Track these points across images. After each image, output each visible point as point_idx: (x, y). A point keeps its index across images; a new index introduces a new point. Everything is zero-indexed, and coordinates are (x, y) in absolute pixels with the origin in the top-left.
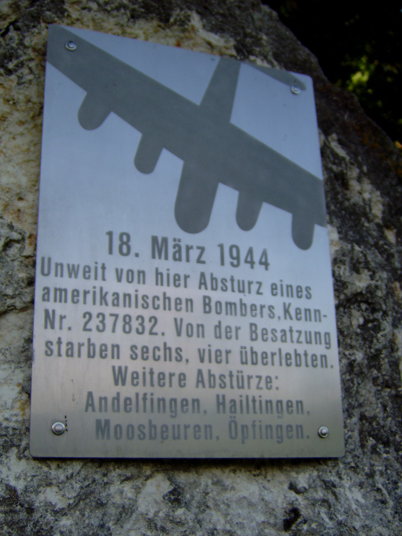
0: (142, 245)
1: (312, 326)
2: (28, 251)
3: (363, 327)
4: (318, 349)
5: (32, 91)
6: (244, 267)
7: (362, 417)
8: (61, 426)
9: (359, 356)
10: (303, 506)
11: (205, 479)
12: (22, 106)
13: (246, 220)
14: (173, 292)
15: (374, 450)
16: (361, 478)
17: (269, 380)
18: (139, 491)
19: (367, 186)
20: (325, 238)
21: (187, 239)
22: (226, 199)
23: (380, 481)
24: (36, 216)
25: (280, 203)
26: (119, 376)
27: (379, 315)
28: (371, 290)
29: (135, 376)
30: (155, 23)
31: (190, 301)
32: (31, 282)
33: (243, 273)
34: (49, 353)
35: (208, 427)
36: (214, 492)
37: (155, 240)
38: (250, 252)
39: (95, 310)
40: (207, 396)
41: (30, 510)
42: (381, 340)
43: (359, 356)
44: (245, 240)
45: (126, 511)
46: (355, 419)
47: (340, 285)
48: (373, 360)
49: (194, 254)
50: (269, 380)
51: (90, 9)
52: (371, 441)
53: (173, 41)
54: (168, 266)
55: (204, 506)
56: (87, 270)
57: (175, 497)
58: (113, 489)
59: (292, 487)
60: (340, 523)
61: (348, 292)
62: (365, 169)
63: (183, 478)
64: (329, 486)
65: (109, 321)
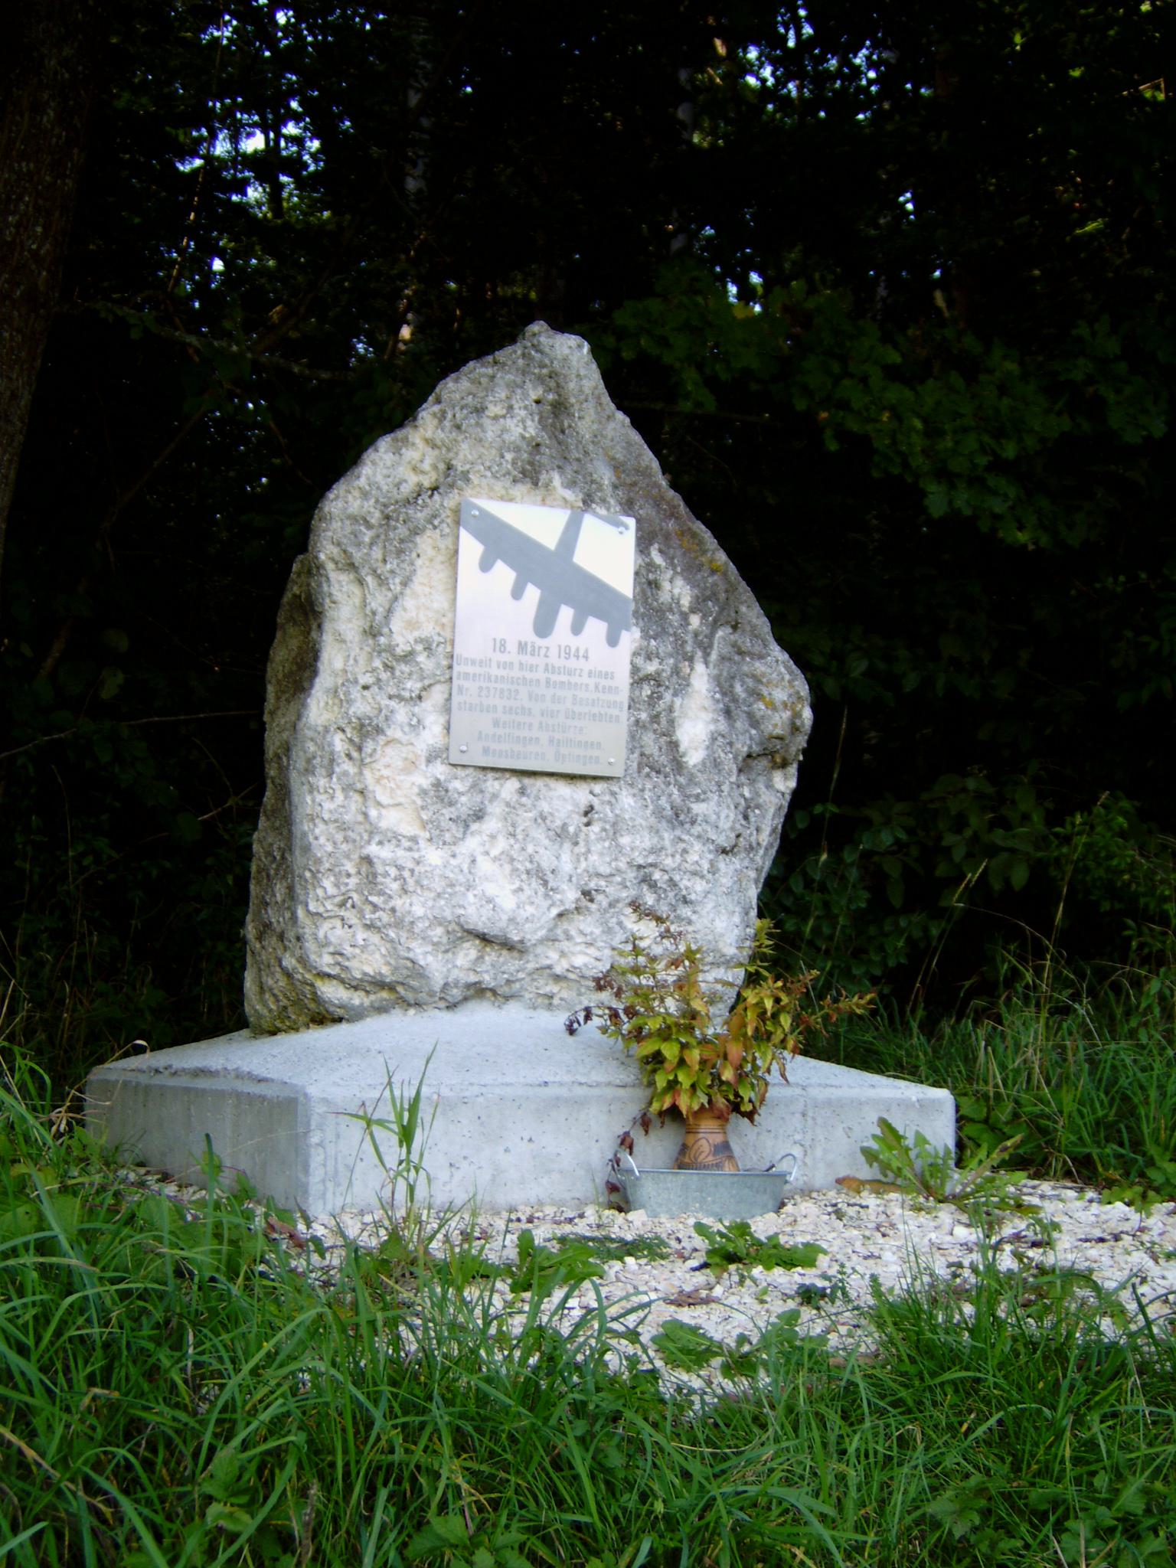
0: (512, 647)
1: (611, 697)
2: (449, 649)
3: (650, 697)
4: (615, 712)
5: (449, 541)
6: (573, 659)
7: (642, 754)
8: (464, 748)
9: (644, 716)
10: (943, 924)
11: (540, 783)
12: (443, 552)
13: (577, 628)
14: (529, 675)
15: (648, 775)
16: (635, 791)
17: (581, 729)
18: (233, 1074)
19: (679, 582)
20: (631, 638)
21: (540, 642)
22: (566, 614)
23: (647, 795)
24: (454, 627)
25: (600, 616)
26: (496, 723)
27: (662, 689)
28: (658, 673)
29: (505, 723)
30: (529, 485)
31: (538, 681)
32: (450, 667)
33: (572, 663)
34: (460, 709)
35: (543, 754)
36: (544, 790)
37: (520, 643)
38: (578, 650)
39: (484, 685)
40: (591, 682)
41: (447, 791)
42: (662, 705)
43: (644, 716)
44: (574, 642)
45: (495, 796)
46: (636, 755)
47: (635, 669)
48: (655, 718)
49: (543, 651)
50: (581, 729)
51: (485, 477)
52: (647, 770)
53: (539, 498)
54: (527, 659)
55: (537, 798)
56: (481, 662)
57: (522, 791)
58: (489, 784)
59: (591, 792)
60: (617, 815)
61: (641, 674)
62: (679, 569)
63: (527, 781)
64: (613, 794)
65: (492, 692)
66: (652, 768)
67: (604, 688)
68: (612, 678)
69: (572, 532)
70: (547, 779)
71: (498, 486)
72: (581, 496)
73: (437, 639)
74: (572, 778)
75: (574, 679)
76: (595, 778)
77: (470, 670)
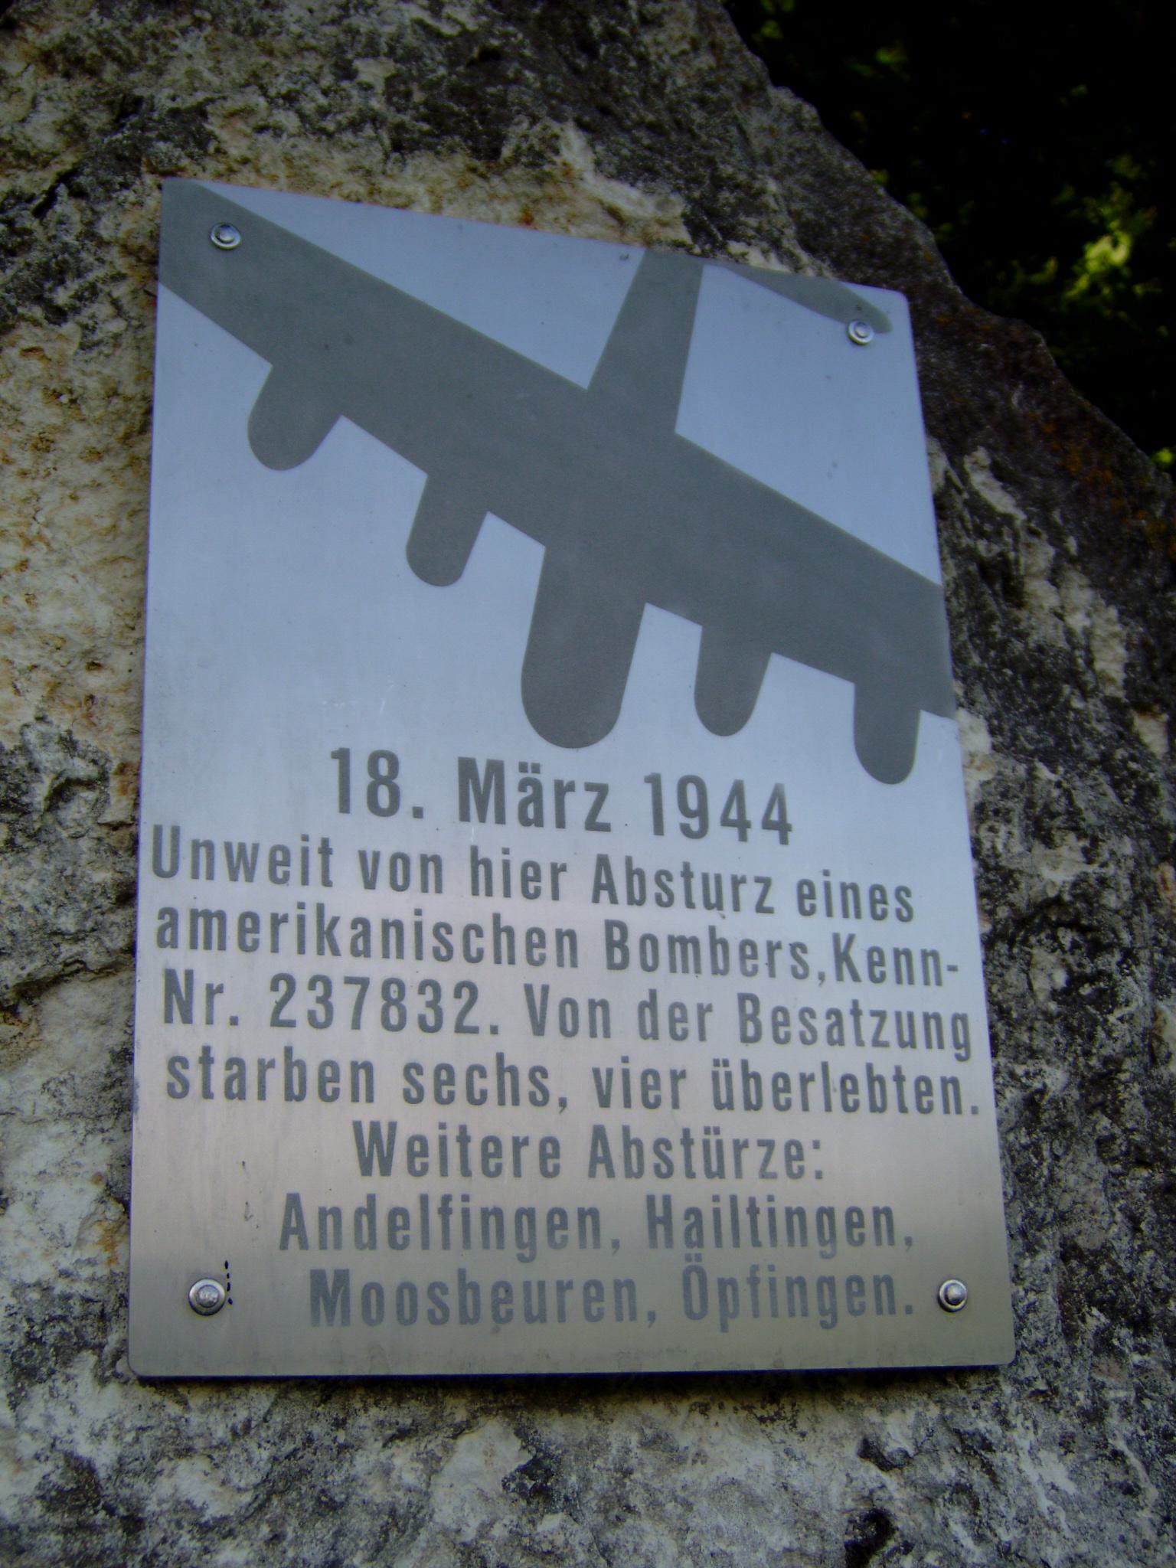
0: (430, 784)
1: (917, 999)
2: (117, 810)
3: (1065, 995)
4: (937, 1063)
6: (721, 836)
7: (1068, 1251)
8: (215, 1291)
9: (1055, 1078)
11: (623, 1430)
12: (94, 407)
13: (724, 704)
14: (519, 913)
15: (1104, 1343)
16: (1067, 1422)
17: (794, 1151)
19: (1080, 593)
20: (951, 749)
21: (558, 763)
22: (666, 650)
23: (1119, 1430)
26: (374, 1149)
27: (1110, 961)
28: (1086, 892)
29: (418, 1147)
30: (460, 160)
31: (567, 937)
32: (127, 895)
33: (718, 853)
34: (178, 1089)
35: (625, 1287)
36: (646, 1467)
38: (737, 792)
39: (304, 968)
41: (134, 1523)
42: (1118, 1031)
43: (1055, 1078)
44: (721, 762)
46: (1046, 1257)
47: (994, 880)
48: (1099, 1086)
49: (579, 804)
51: (278, 131)
52: (1096, 1319)
54: (507, 840)
55: (617, 1508)
56: (280, 858)
57: (537, 1484)
59: (870, 1451)
61: (1020, 898)
62: (1072, 544)
63: (557, 1429)
64: (973, 1447)
65: (343, 998)
66: (1110, 1308)
67: (875, 957)
68: (906, 915)
69: (650, 350)
70: (656, 1412)
71: (334, 165)
72: (678, 207)
73: (50, 758)
74: (769, 1392)
75: (736, 926)
76: (882, 1383)
77: (229, 896)
